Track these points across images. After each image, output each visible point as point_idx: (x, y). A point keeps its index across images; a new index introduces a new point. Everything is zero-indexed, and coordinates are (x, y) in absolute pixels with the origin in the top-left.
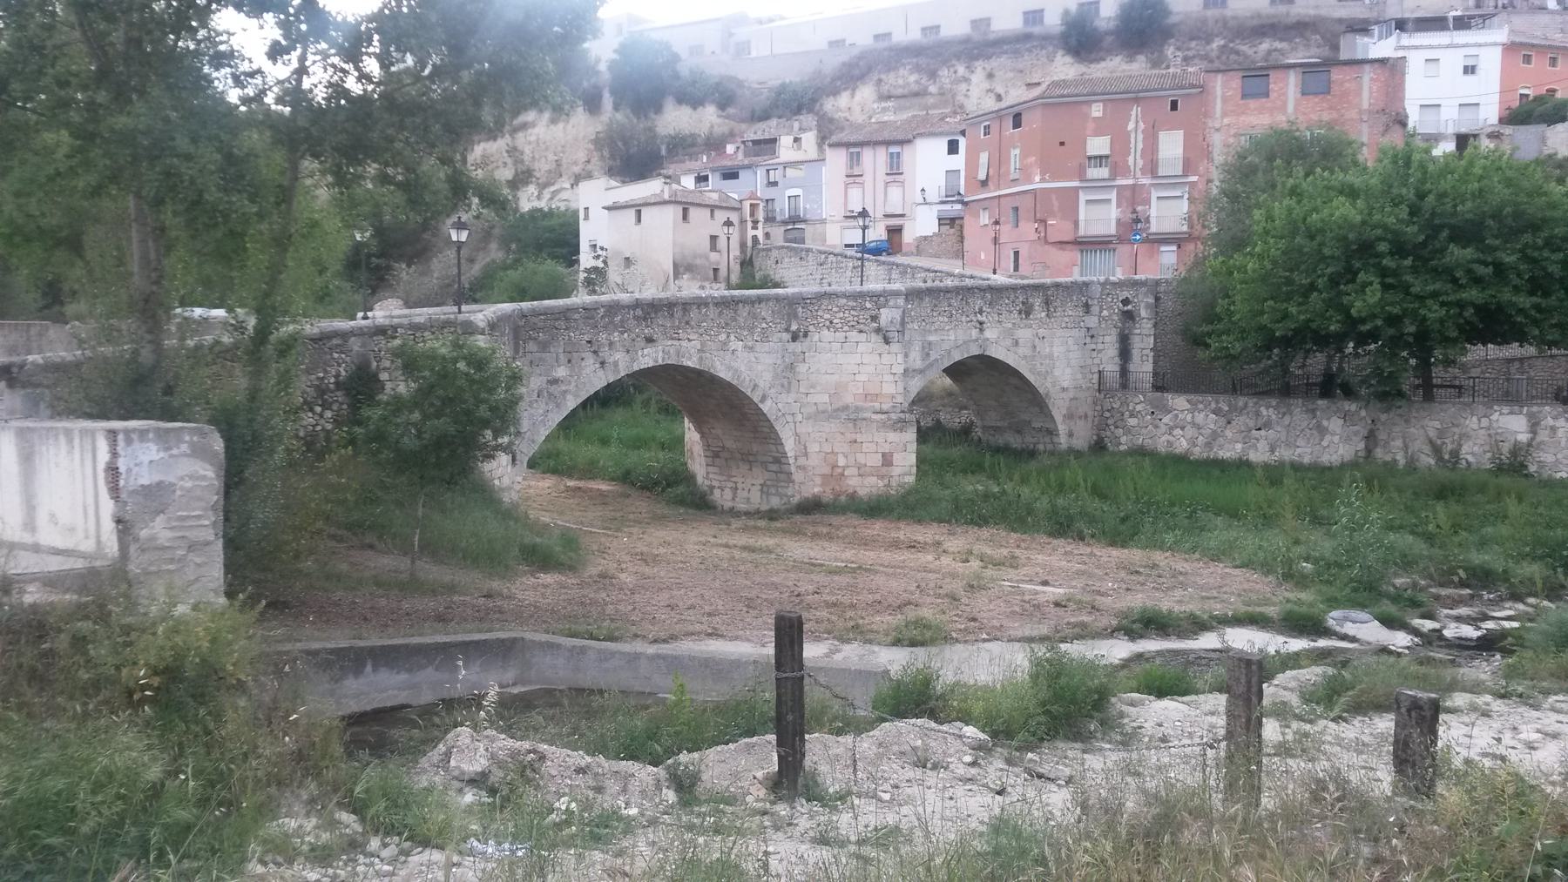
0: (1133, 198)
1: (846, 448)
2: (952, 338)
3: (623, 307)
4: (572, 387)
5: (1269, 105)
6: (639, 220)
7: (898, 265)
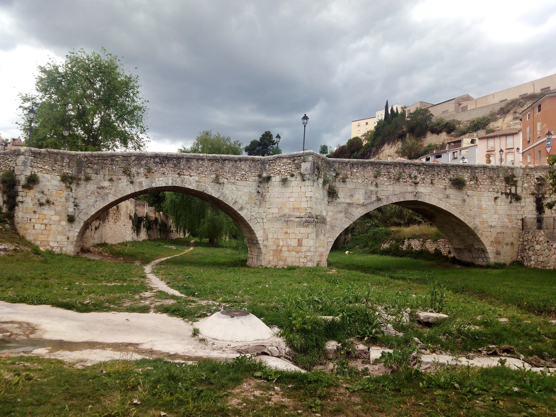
1: (283, 236)
2: (392, 190)
3: (147, 157)
4: (112, 191)
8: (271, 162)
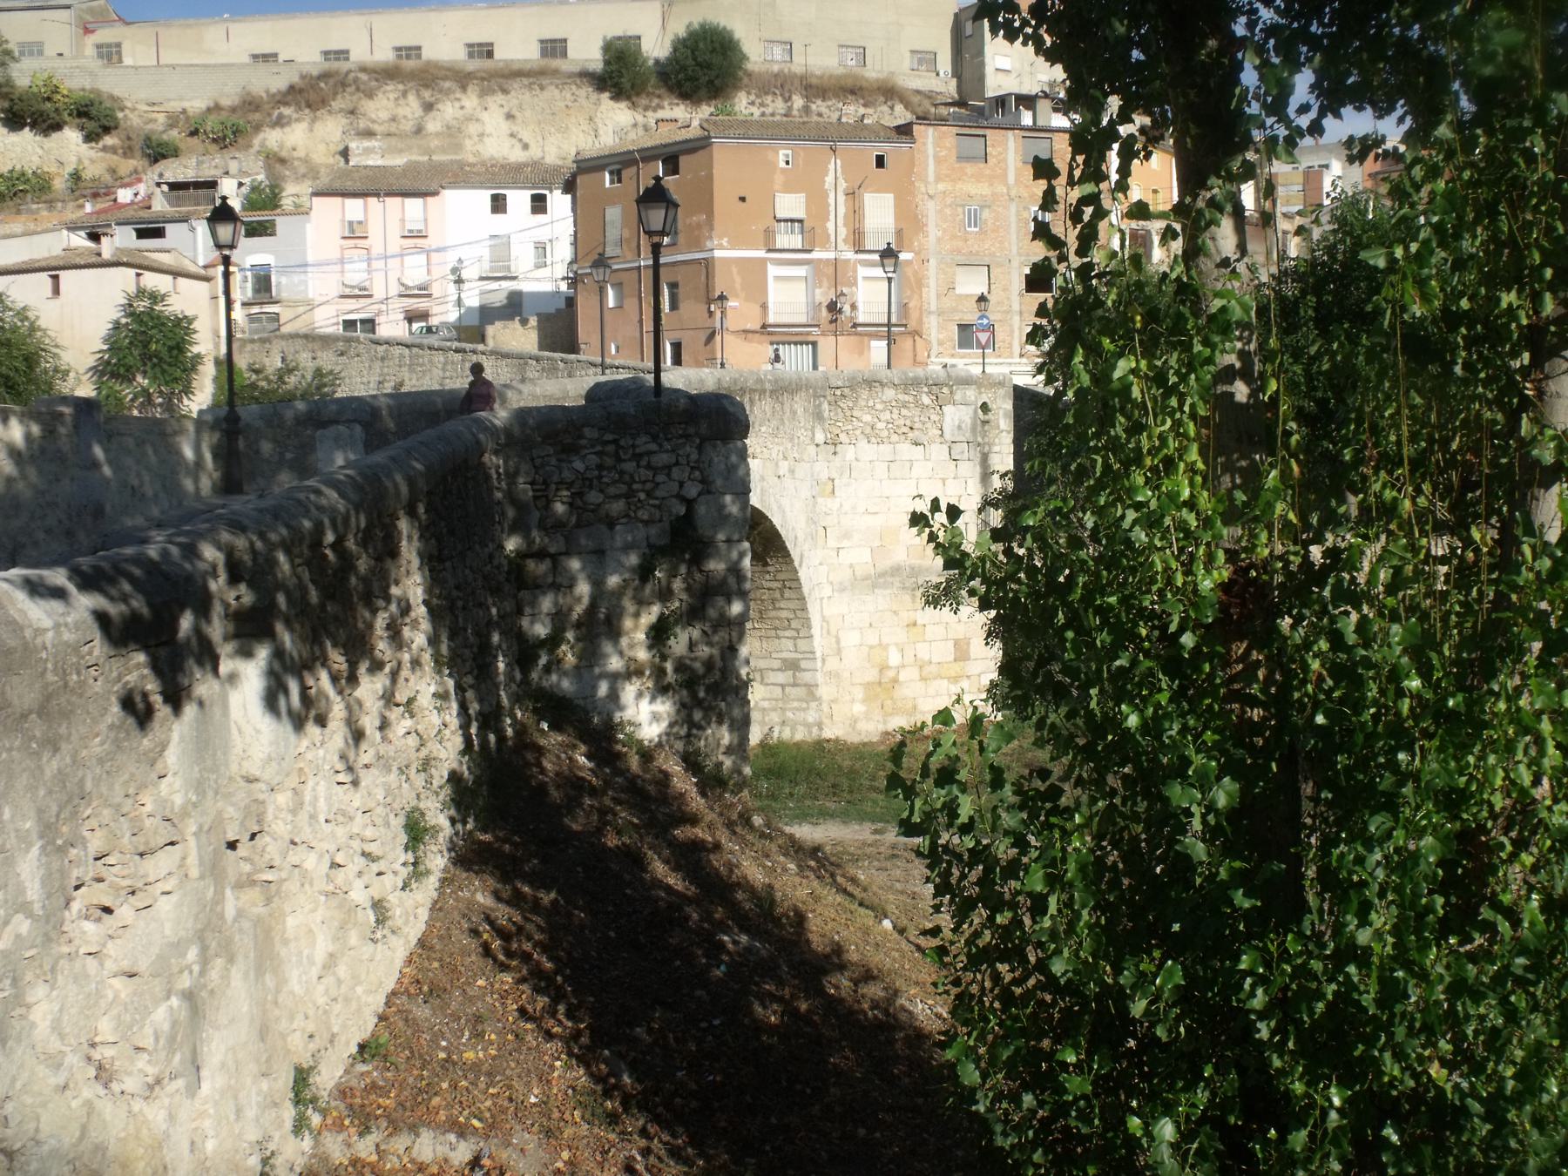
5: (988, 172)
6: (56, 291)
8: (838, 392)
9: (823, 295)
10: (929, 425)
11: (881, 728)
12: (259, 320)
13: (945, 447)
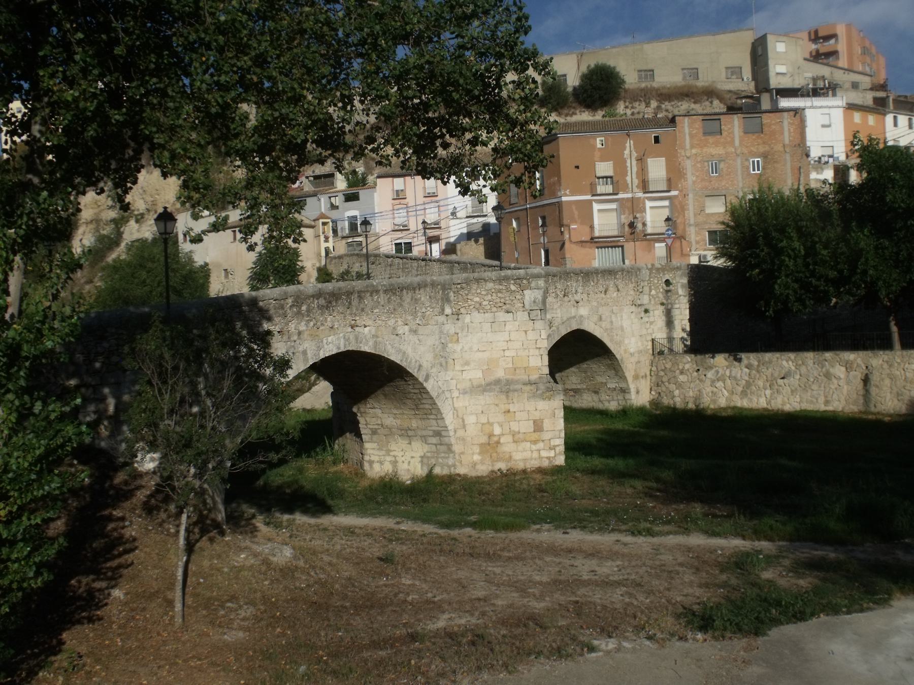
0: (634, 207)
1: (501, 418)
2: (559, 315)
7: (459, 263)
8: (459, 286)
9: (626, 219)
10: (515, 301)
11: (490, 468)
12: (352, 245)
13: (526, 313)
